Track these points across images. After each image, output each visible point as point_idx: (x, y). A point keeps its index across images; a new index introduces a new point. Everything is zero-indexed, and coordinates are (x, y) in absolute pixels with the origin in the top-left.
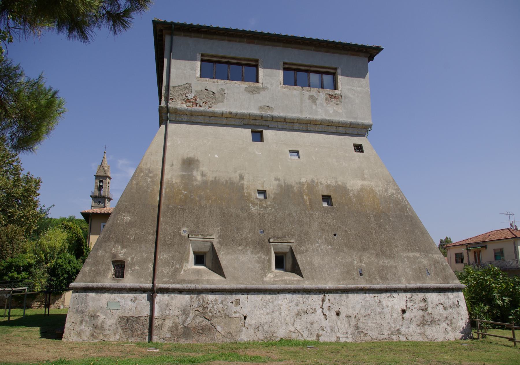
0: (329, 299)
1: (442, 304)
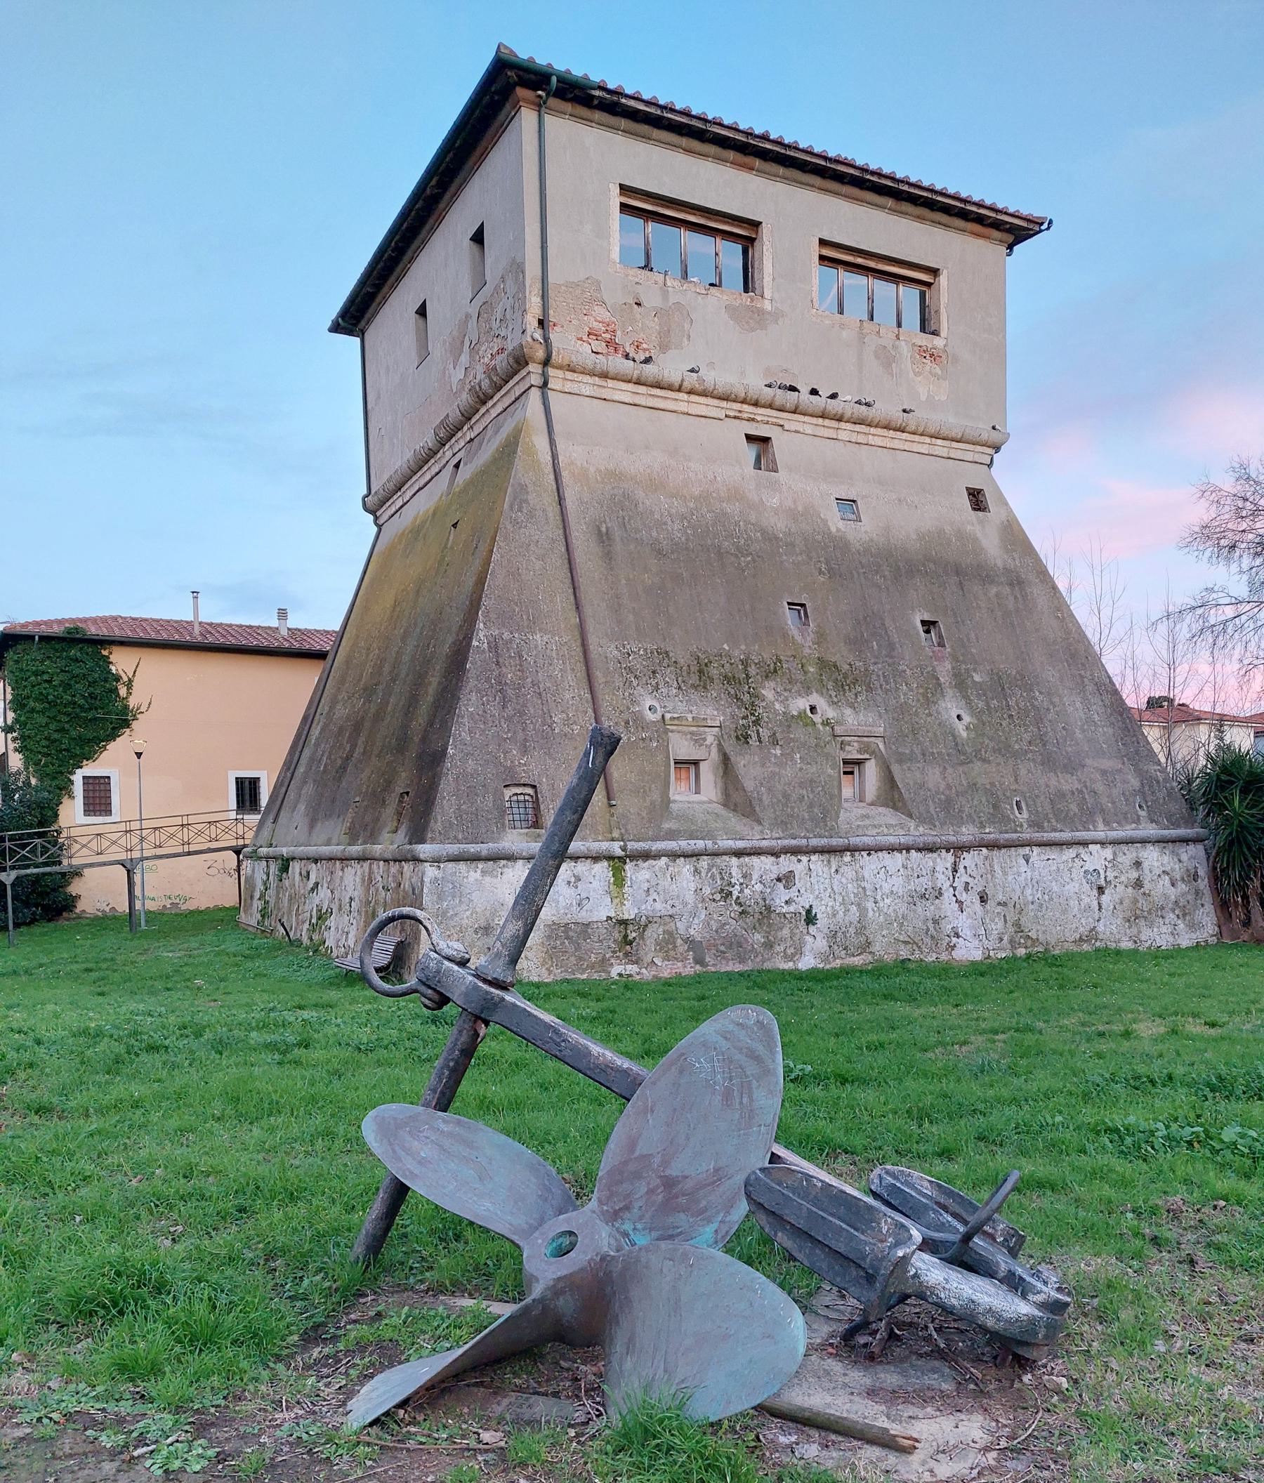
0: (965, 867)
1: (1168, 874)
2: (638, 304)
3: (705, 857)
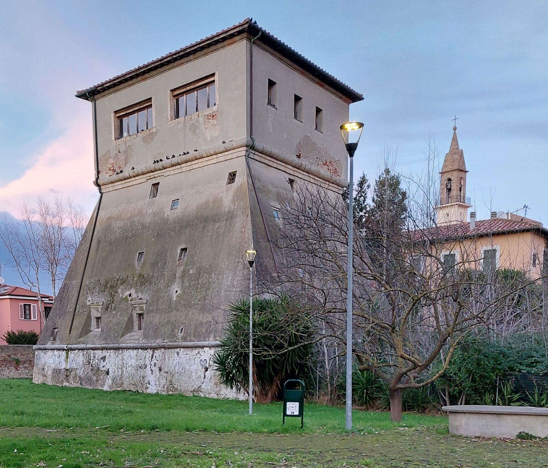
2: (120, 152)
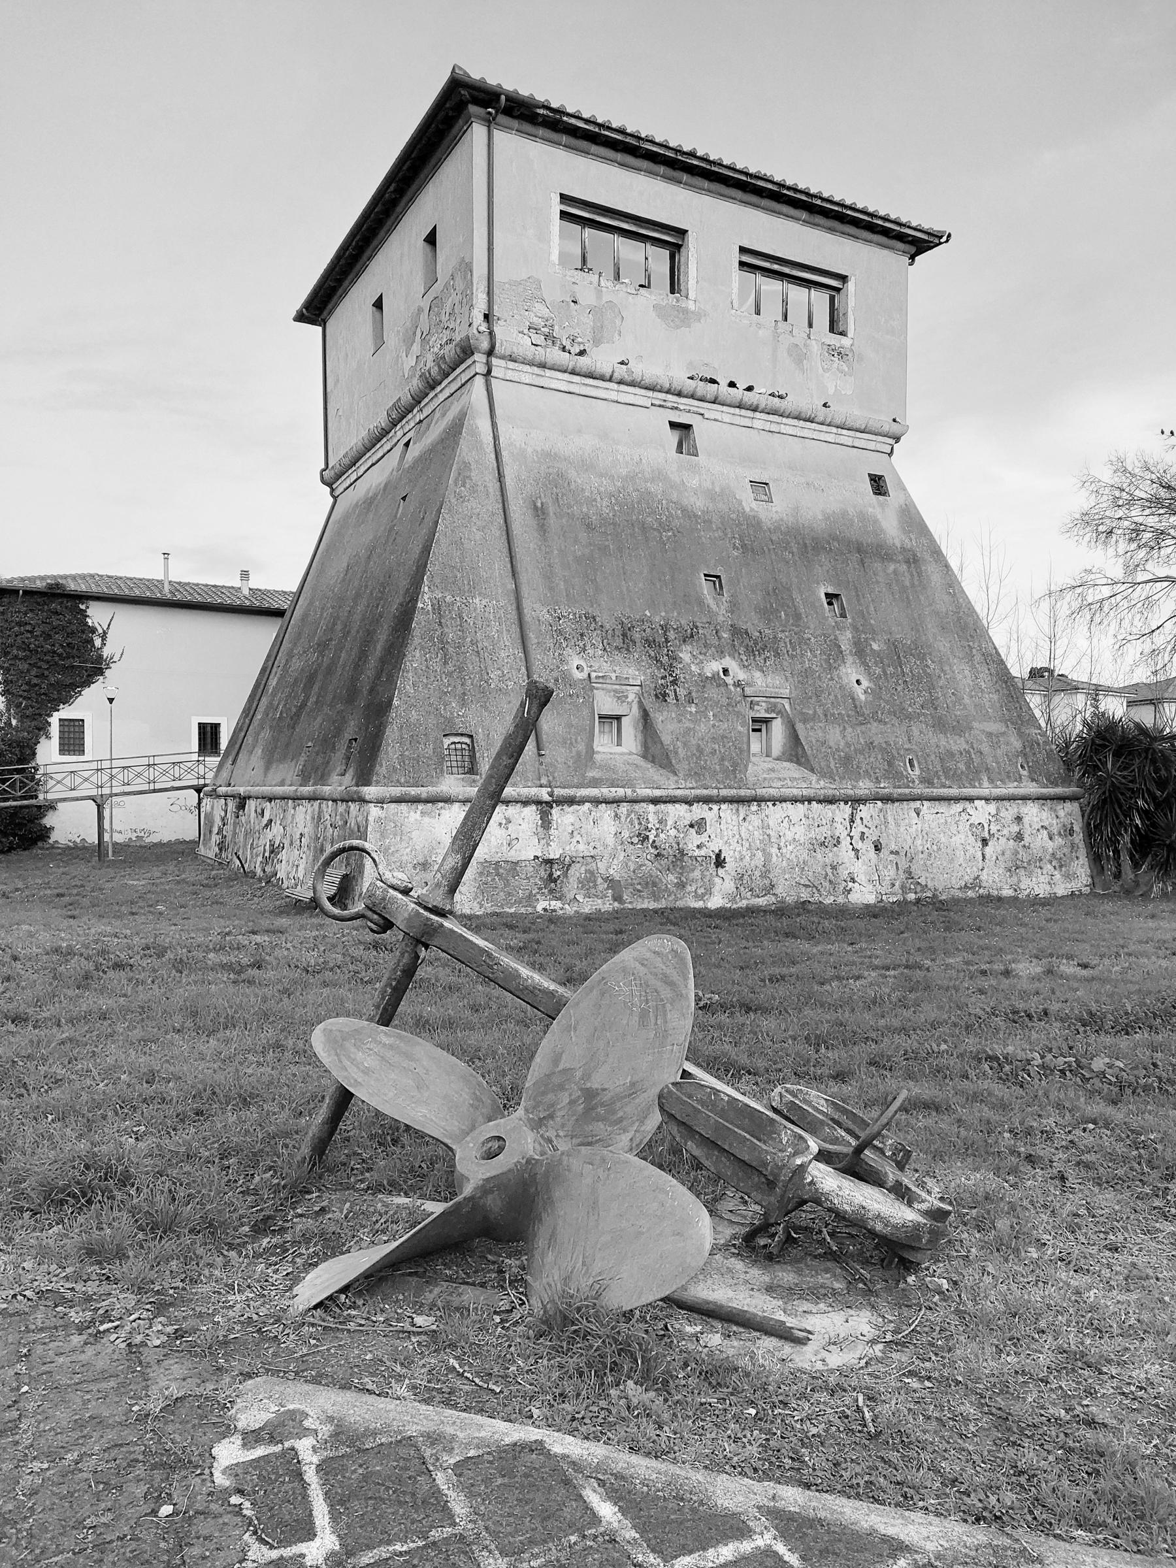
3: (625, 804)
